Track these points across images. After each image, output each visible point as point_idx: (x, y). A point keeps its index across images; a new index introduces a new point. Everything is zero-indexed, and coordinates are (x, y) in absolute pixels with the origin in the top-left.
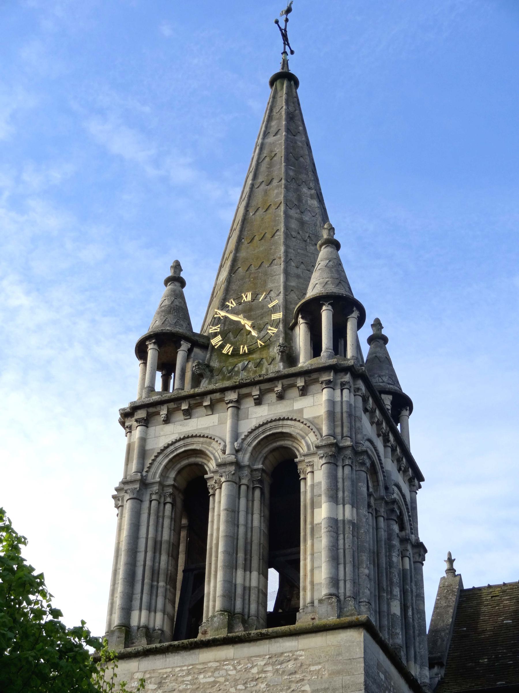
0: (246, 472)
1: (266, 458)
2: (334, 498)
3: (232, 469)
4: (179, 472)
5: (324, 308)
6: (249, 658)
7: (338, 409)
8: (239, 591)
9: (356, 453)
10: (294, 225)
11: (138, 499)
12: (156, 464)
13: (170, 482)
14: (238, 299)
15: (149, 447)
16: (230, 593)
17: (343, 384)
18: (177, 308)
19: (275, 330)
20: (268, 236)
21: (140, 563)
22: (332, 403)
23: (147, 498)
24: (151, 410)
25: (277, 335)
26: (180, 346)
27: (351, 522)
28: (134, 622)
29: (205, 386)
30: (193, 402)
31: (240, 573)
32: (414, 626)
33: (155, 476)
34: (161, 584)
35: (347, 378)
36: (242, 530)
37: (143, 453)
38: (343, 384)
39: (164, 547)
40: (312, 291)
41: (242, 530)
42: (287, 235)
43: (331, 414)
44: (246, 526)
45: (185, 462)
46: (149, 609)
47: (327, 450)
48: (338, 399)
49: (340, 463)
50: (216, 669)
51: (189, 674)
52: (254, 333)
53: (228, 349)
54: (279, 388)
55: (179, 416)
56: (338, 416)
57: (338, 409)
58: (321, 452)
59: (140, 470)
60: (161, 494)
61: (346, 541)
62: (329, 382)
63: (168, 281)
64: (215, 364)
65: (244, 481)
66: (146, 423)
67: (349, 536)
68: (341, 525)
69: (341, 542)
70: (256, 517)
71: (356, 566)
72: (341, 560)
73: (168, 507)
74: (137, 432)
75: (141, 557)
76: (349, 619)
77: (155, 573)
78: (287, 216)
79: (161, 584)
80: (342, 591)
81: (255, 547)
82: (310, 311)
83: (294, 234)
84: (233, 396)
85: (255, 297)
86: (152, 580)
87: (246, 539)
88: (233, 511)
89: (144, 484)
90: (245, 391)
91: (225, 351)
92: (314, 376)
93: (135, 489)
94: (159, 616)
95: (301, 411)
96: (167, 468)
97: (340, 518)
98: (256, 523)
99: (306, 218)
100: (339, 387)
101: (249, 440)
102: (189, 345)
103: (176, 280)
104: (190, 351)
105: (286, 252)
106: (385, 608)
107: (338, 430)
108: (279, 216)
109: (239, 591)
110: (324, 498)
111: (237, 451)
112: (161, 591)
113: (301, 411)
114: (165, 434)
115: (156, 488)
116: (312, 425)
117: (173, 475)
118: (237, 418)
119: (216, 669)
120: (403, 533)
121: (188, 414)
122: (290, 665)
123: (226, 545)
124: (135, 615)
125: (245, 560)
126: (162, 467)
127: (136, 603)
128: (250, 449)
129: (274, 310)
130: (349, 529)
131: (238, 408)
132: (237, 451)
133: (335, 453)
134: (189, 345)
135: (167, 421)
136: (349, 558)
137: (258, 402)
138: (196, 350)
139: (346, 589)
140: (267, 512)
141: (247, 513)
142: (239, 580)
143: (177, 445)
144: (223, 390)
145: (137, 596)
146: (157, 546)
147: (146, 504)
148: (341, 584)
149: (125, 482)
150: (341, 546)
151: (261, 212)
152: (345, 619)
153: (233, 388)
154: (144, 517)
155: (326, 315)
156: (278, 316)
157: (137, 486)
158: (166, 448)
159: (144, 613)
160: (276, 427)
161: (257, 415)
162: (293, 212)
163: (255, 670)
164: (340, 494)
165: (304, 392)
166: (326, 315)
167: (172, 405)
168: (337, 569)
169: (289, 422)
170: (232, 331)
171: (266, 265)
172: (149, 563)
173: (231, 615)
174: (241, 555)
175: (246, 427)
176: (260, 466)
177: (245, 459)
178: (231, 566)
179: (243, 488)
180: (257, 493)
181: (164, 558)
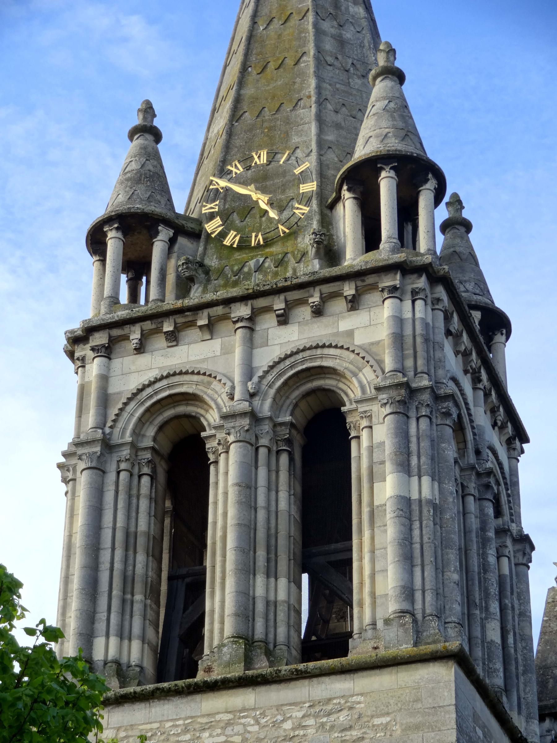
0: (266, 427)
1: (296, 406)
2: (404, 466)
3: (246, 422)
4: (161, 428)
5: (383, 174)
6: (279, 707)
7: (408, 331)
8: (260, 607)
9: (437, 398)
10: (329, 45)
11: (99, 469)
12: (125, 415)
13: (148, 442)
14: (246, 160)
15: (112, 390)
16: (246, 611)
17: (415, 293)
18: (150, 175)
19: (306, 209)
20: (290, 62)
21: (105, 566)
22: (399, 321)
23: (112, 468)
24: (116, 332)
25: (308, 217)
26: (157, 233)
27: (430, 502)
28: (98, 655)
29: (196, 296)
30: (180, 320)
31: (260, 580)
32: (516, 659)
33: (124, 433)
34: (138, 597)
35: (422, 282)
36: (261, 515)
37: (105, 400)
38: (415, 293)
39: (141, 541)
40: (362, 151)
41: (261, 515)
42: (320, 62)
43: (398, 339)
44: (268, 508)
45: (169, 413)
46: (121, 636)
47: (393, 393)
48: (408, 315)
49: (413, 414)
50: (229, 723)
51: (186, 731)
52: (273, 214)
53: (232, 239)
54: (315, 299)
55: (160, 342)
56: (409, 341)
57: (408, 331)
58: (383, 396)
59: (101, 425)
60: (133, 460)
61: (425, 532)
62: (394, 289)
63: (134, 133)
64: (212, 262)
65: (264, 441)
66: (107, 351)
67: (428, 522)
68: (415, 507)
69: (416, 533)
70: (283, 496)
71: (440, 568)
72: (418, 561)
73: (146, 480)
74: (95, 367)
75: (105, 556)
76: (431, 648)
77: (128, 582)
78: (319, 32)
79: (138, 597)
80: (418, 606)
81: (282, 542)
82: (362, 179)
83: (330, 59)
84: (242, 311)
85: (272, 157)
86: (124, 592)
87: (268, 536)
88: (248, 486)
89: (108, 446)
90: (261, 302)
91: (227, 242)
92: (370, 279)
93: (93, 453)
94: (136, 645)
95: (350, 334)
96: (142, 422)
97: (415, 496)
98: (283, 505)
99: (348, 34)
100: (409, 296)
101: (270, 378)
102: (171, 233)
103: (148, 131)
104: (172, 241)
105: (319, 88)
106: (477, 632)
107: (409, 363)
108: (306, 31)
109: (260, 607)
110: (389, 467)
111: (252, 395)
112: (138, 608)
113: (350, 334)
114: (136, 371)
115: (126, 452)
116: (368, 355)
117: (151, 431)
118: (250, 344)
119: (229, 723)
120: (500, 521)
121: (173, 338)
122: (343, 718)
123: (239, 538)
124: (99, 643)
125: (268, 560)
126: (134, 420)
127: (101, 626)
128: (272, 392)
129: (303, 178)
130: (428, 513)
131: (251, 330)
132: (252, 395)
133: (405, 397)
134: (171, 233)
135: (140, 349)
136: (429, 557)
137: (283, 320)
138: (182, 241)
139: (426, 603)
140: (299, 489)
141: (269, 489)
142: (260, 591)
143: (158, 385)
144: (228, 302)
145: (102, 616)
146: (130, 540)
147: (111, 477)
148: (418, 595)
149: (78, 444)
150: (417, 539)
151: (276, 24)
152: (425, 649)
153: (243, 299)
154: (109, 496)
155: (387, 186)
156: (309, 187)
157: (97, 449)
158: (140, 391)
159: (113, 641)
160: (312, 359)
161: (281, 340)
162: (327, 26)
163: (288, 725)
164: (414, 461)
165: (354, 304)
166: (387, 186)
167: (148, 325)
168: (411, 573)
169: (332, 351)
170: (237, 210)
171: (287, 108)
172: (118, 566)
173: (247, 641)
174: (261, 554)
175: (264, 358)
176: (288, 418)
177: (265, 407)
178: (247, 570)
179: (263, 452)
180: (284, 459)
181: (141, 558)
